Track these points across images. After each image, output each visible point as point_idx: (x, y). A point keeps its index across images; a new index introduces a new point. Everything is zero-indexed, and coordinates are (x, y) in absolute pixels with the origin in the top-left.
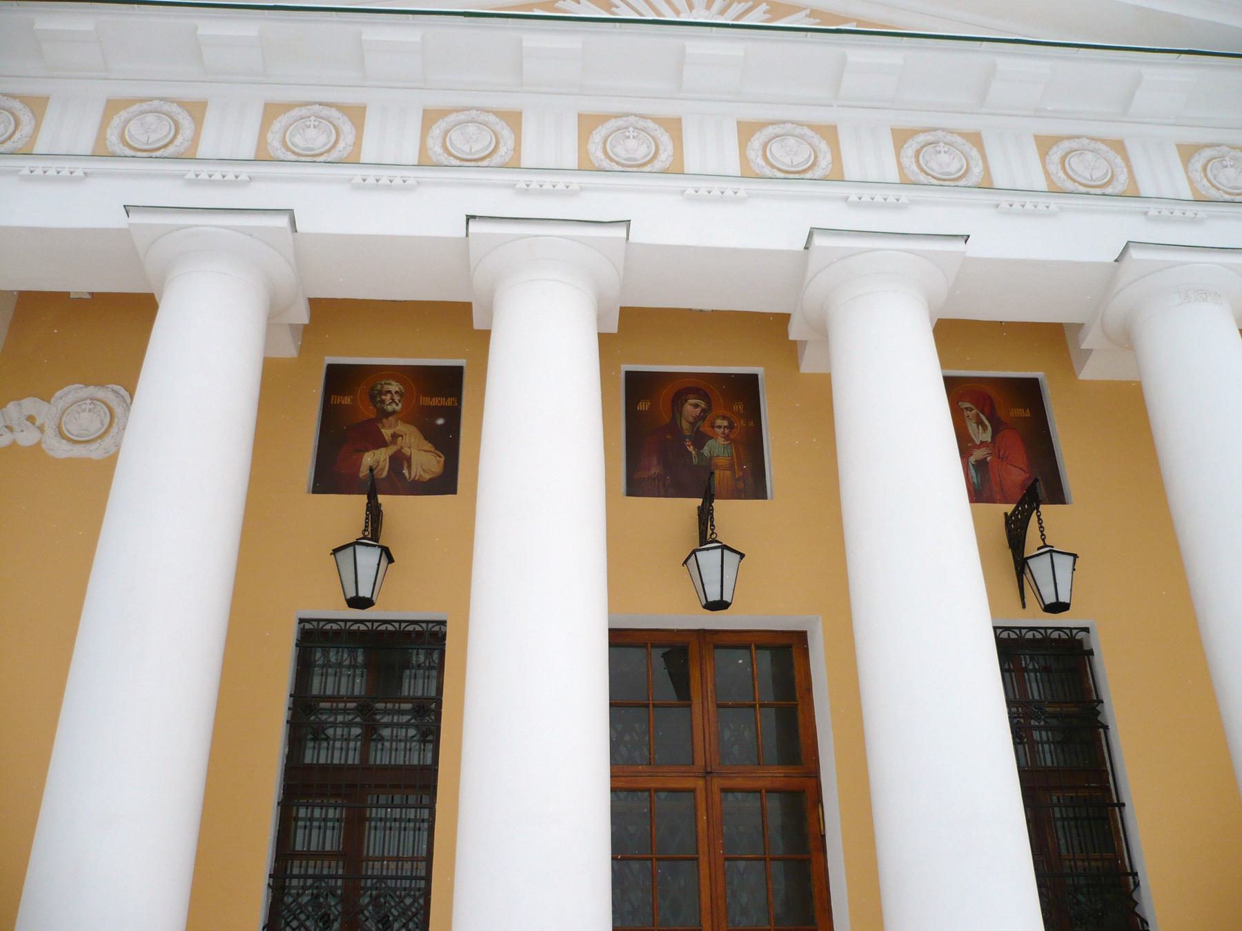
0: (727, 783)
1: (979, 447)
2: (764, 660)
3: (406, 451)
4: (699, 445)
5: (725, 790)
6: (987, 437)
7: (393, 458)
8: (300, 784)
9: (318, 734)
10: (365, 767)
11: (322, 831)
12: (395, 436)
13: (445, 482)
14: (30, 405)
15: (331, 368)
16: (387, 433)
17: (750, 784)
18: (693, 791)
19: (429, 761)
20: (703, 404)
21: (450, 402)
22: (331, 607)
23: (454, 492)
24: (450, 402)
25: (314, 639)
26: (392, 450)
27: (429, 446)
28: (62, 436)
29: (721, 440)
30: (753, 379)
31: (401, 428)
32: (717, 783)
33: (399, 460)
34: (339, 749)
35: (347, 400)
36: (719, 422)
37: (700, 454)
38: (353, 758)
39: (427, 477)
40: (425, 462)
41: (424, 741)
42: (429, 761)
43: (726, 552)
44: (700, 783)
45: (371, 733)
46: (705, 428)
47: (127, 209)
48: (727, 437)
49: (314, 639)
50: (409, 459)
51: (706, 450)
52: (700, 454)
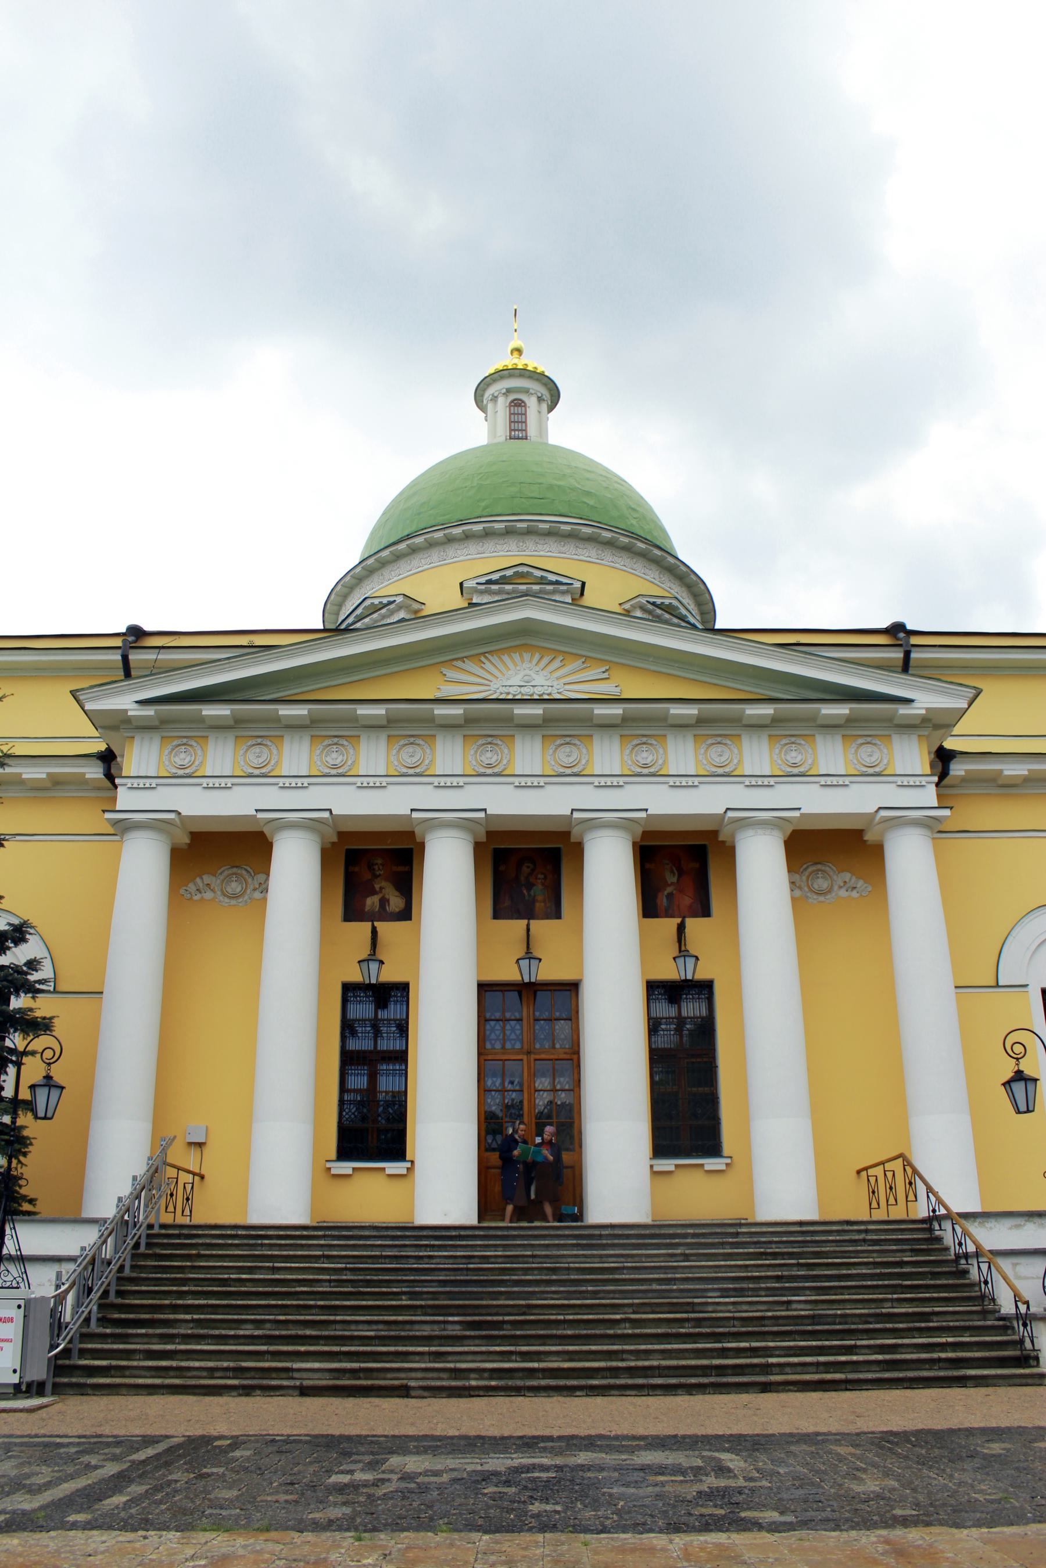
0: (538, 1057)
1: (669, 885)
2: (351, 1070)
3: (387, 896)
4: (529, 889)
5: (536, 1060)
6: (674, 880)
7: (380, 900)
8: (349, 1059)
9: (354, 1033)
10: (375, 1051)
11: (358, 1081)
12: (381, 888)
13: (406, 914)
14: (207, 879)
15: (347, 850)
16: (377, 887)
17: (547, 1057)
18: (521, 1060)
19: (704, 1013)
20: (532, 866)
21: (407, 869)
22: (355, 976)
23: (410, 919)
24: (407, 869)
25: (349, 990)
26: (380, 896)
27: (397, 894)
28: (225, 895)
29: (540, 887)
30: (559, 849)
31: (384, 884)
32: (533, 1057)
33: (384, 902)
34: (362, 1044)
35: (356, 869)
36: (540, 876)
37: (529, 895)
38: (371, 1047)
39: (397, 910)
40: (396, 903)
41: (401, 1036)
42: (704, 1013)
43: (197, 1171)
44: (525, 1057)
45: (377, 1033)
46: (532, 880)
47: (257, 811)
48: (543, 884)
49: (349, 990)
50: (388, 901)
51: (532, 893)
52: (529, 895)
